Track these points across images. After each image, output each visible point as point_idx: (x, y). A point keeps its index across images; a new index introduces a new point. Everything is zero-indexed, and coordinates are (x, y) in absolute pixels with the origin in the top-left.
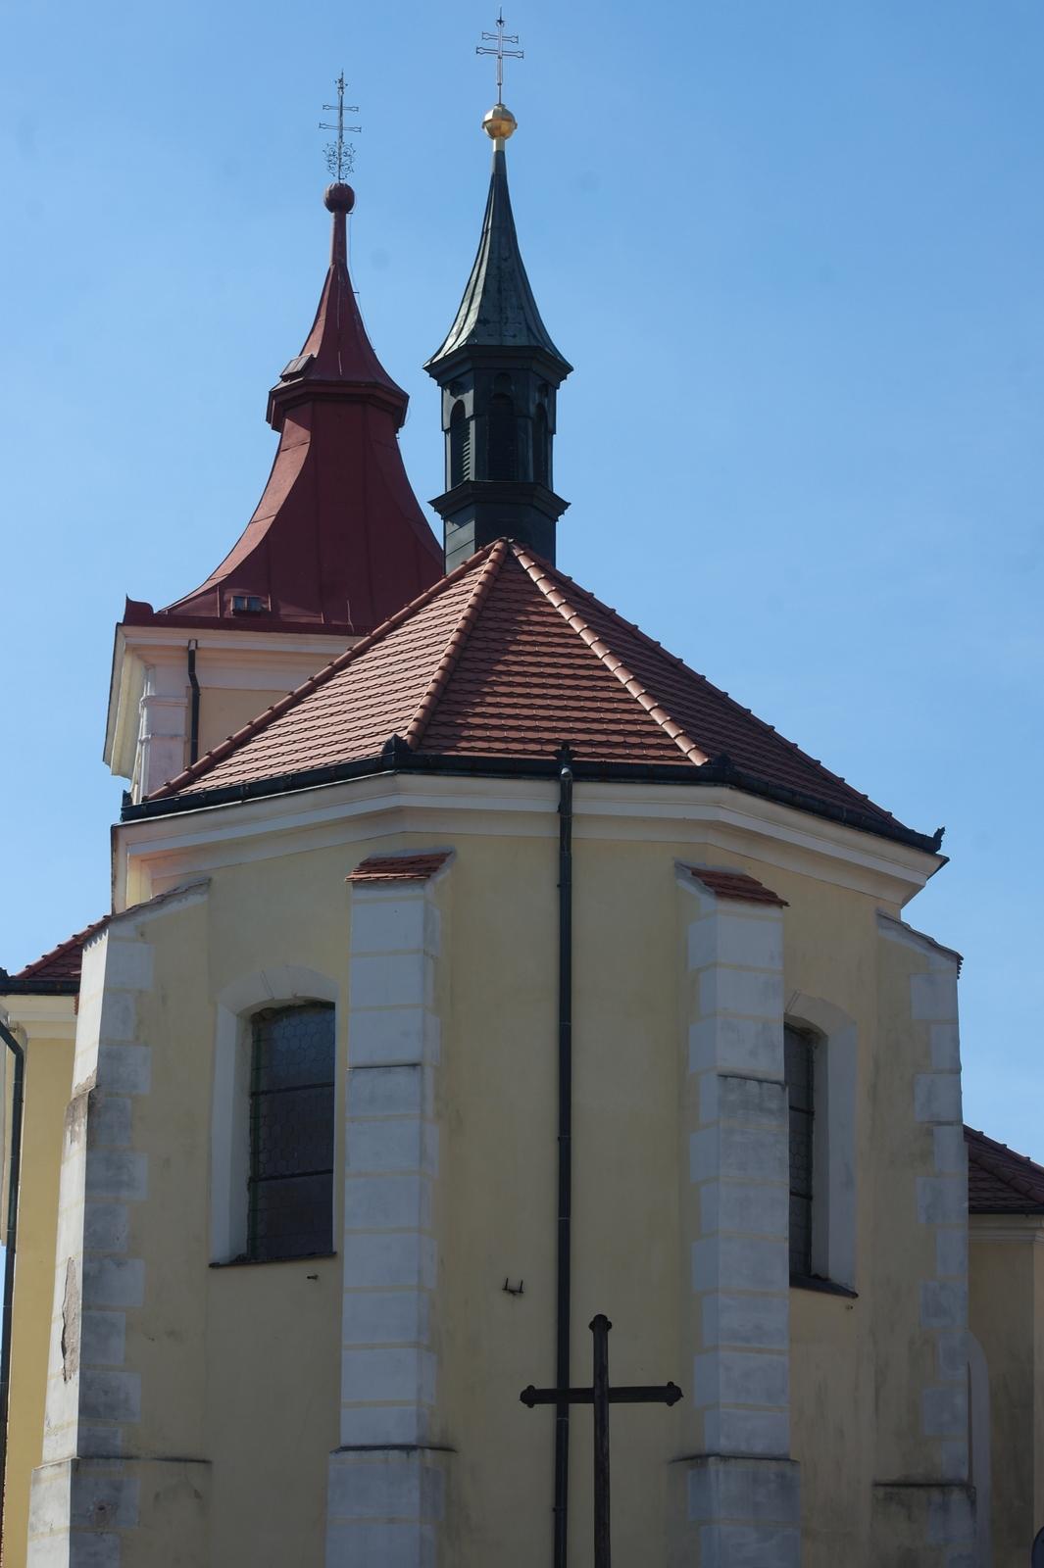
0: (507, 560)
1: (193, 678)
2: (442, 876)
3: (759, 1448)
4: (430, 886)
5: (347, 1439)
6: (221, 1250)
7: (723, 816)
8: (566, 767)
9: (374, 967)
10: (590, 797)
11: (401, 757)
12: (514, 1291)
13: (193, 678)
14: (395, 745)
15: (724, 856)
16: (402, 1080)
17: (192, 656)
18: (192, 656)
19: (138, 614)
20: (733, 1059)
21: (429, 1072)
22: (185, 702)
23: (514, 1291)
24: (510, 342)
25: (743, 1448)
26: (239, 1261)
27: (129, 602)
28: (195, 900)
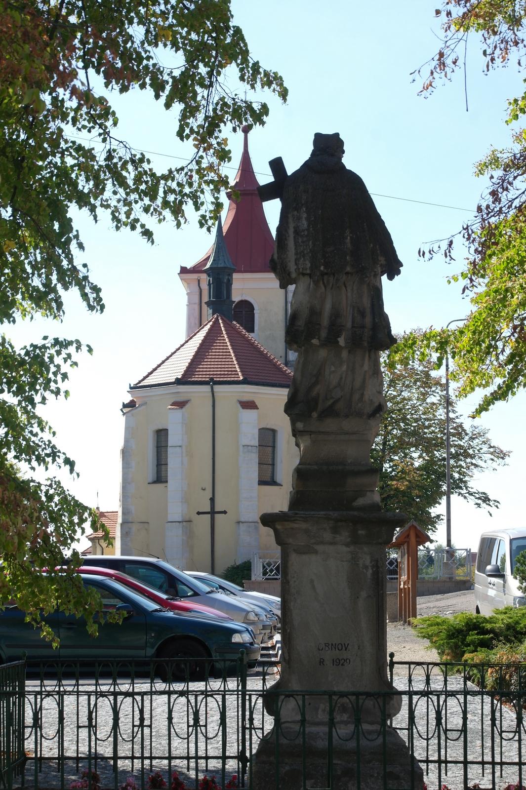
0: (217, 319)
1: (200, 287)
2: (187, 406)
3: (250, 520)
4: (184, 409)
5: (169, 520)
6: (150, 480)
7: (246, 390)
8: (212, 382)
9: (174, 422)
10: (217, 388)
11: (178, 382)
12: (204, 490)
13: (200, 287)
14: (177, 379)
15: (247, 398)
16: (178, 449)
17: (199, 281)
18: (199, 281)
19: (184, 270)
20: (245, 441)
21: (184, 447)
22: (198, 293)
23: (204, 490)
24: (219, 266)
25: (247, 520)
26: (154, 482)
27: (181, 267)
28: (144, 407)
